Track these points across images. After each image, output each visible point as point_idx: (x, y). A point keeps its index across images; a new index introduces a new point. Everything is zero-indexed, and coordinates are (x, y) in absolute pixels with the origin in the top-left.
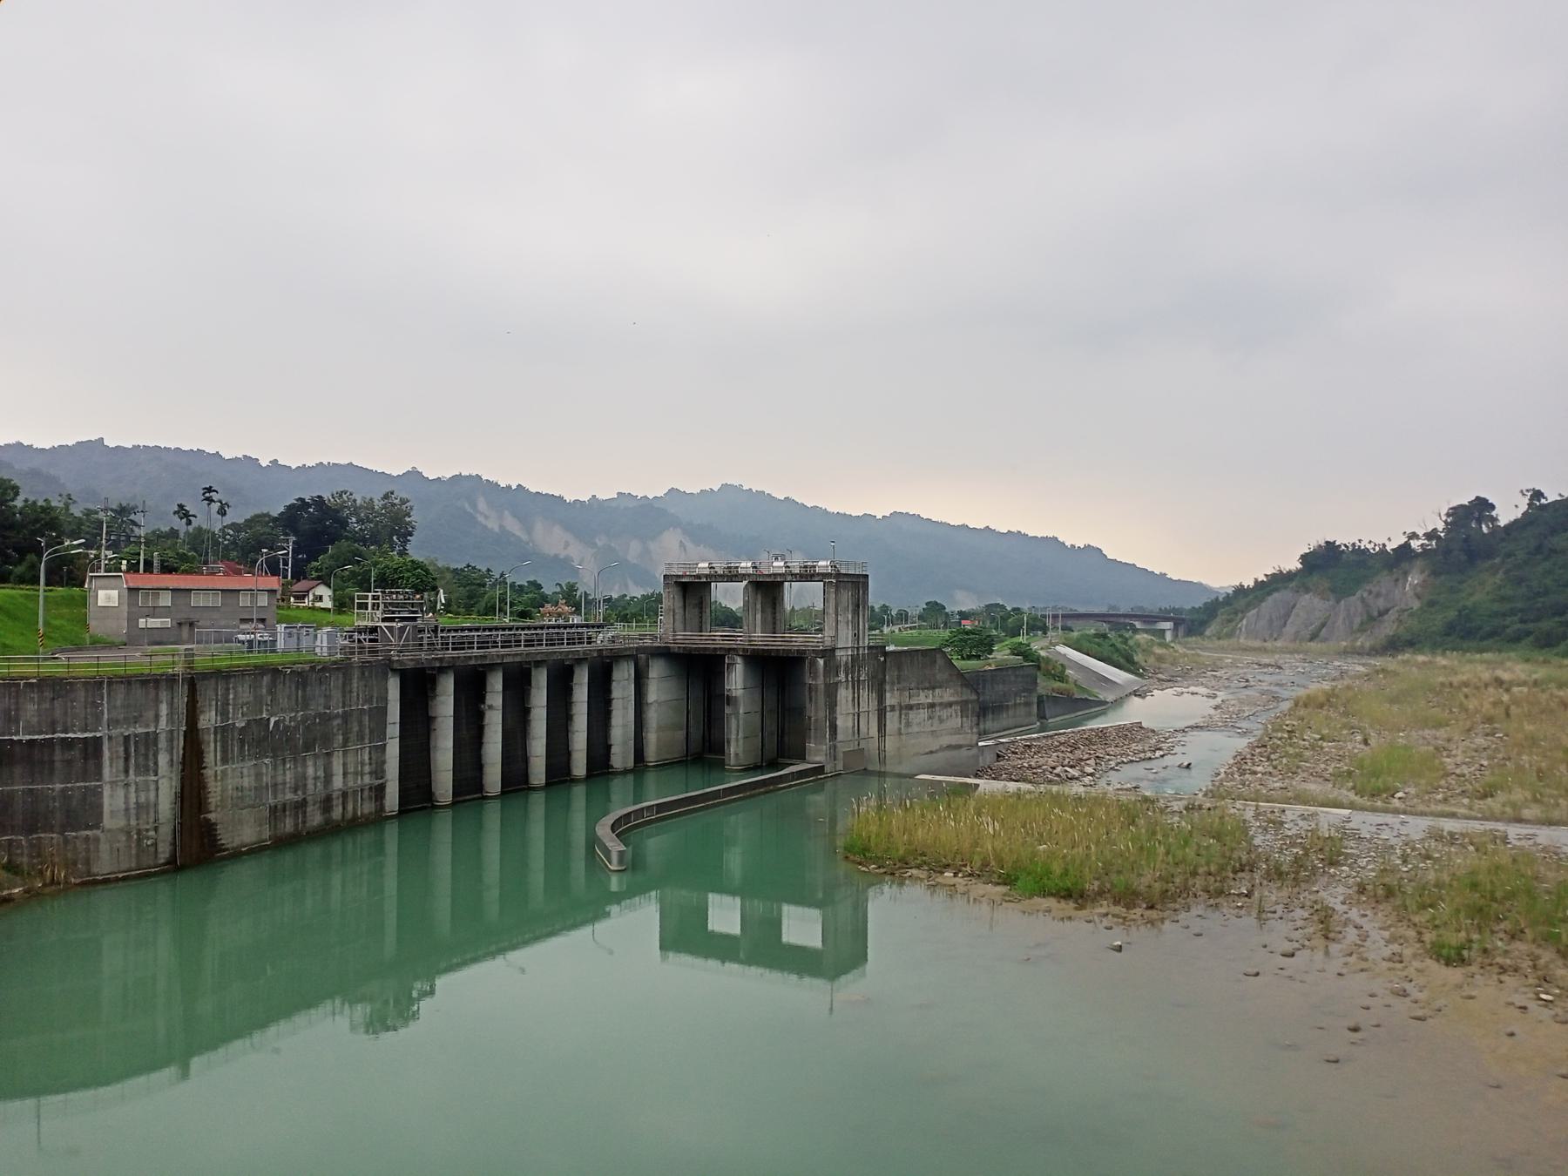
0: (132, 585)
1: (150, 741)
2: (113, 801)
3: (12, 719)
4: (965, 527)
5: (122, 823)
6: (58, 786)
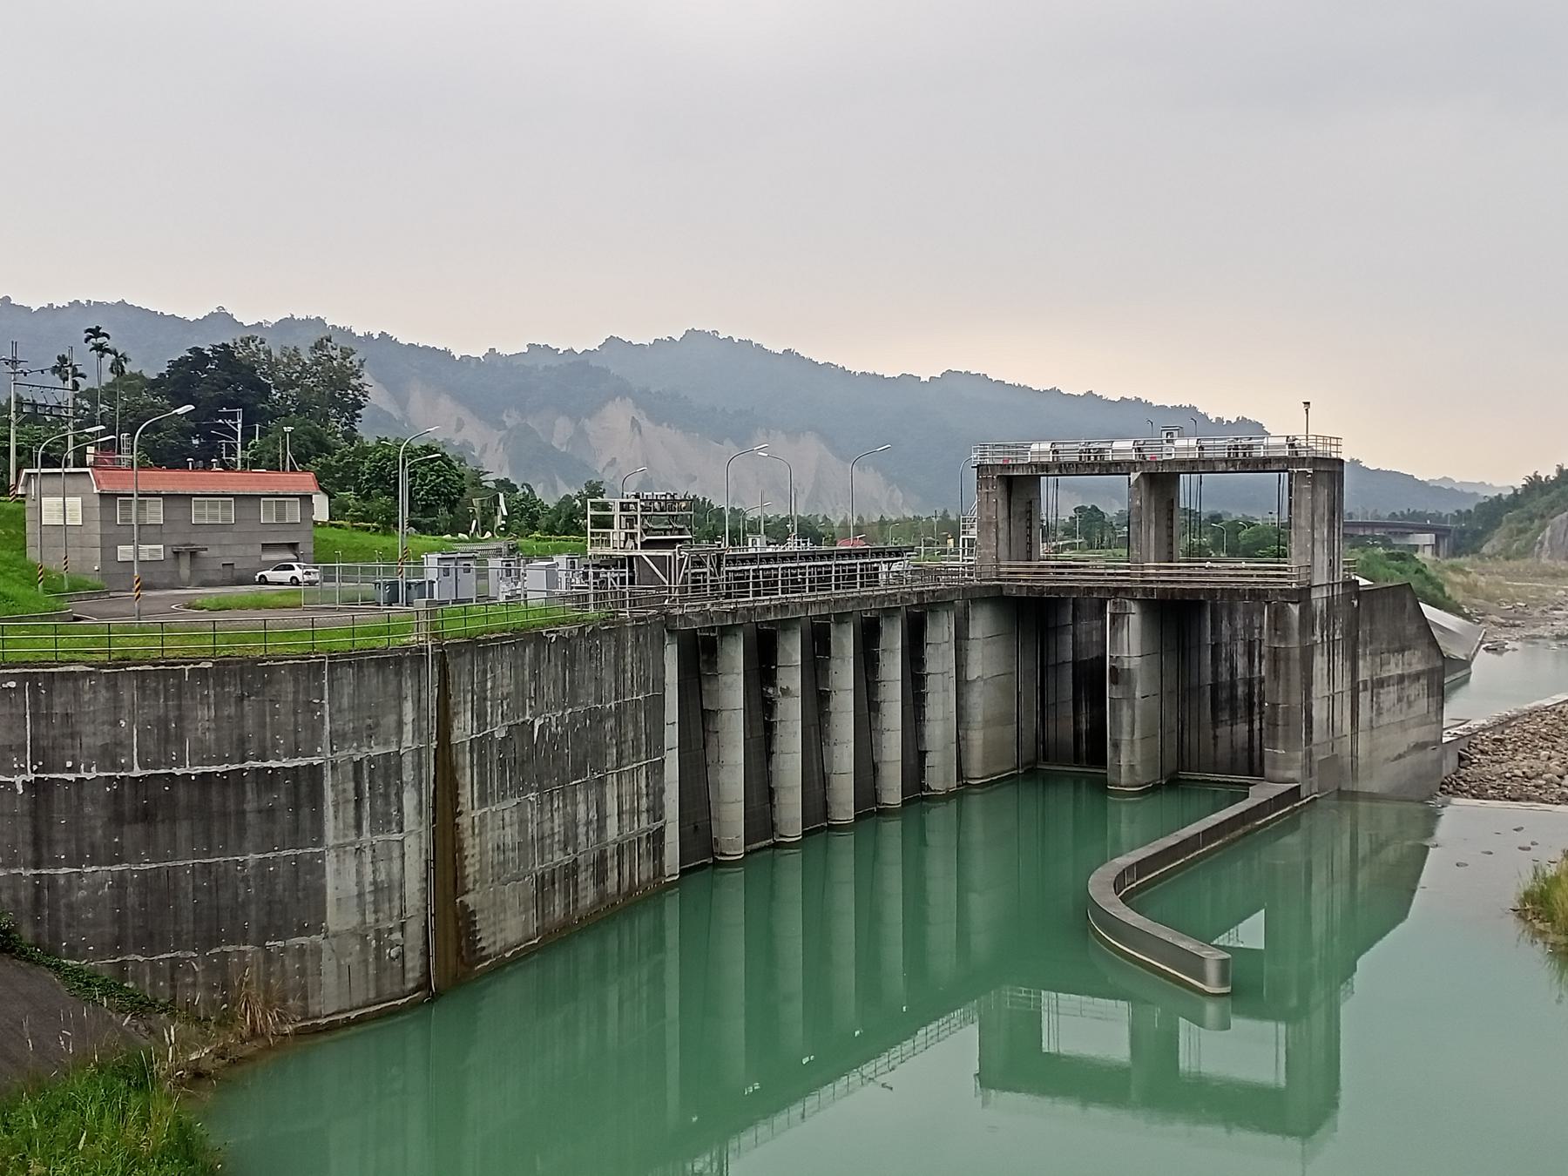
0: (107, 489)
1: (390, 768)
2: (341, 880)
4: (1055, 392)
5: (354, 920)
6: (252, 858)
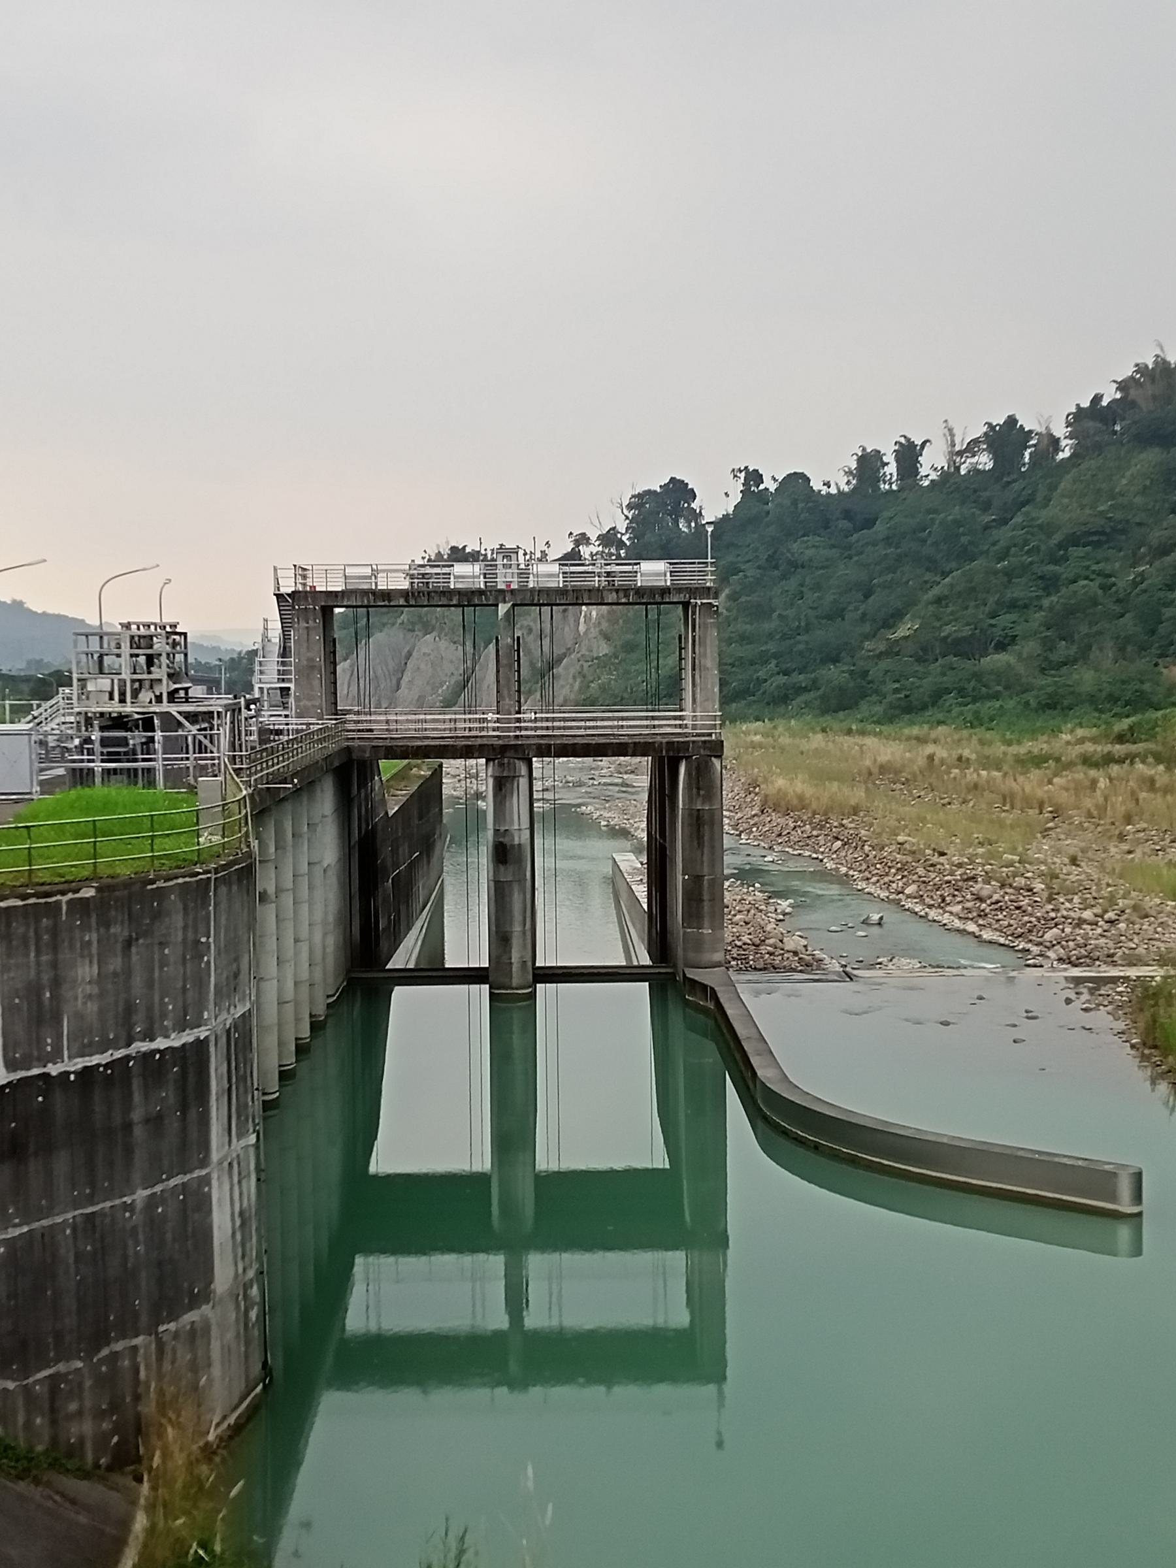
3: (39, 1016)
